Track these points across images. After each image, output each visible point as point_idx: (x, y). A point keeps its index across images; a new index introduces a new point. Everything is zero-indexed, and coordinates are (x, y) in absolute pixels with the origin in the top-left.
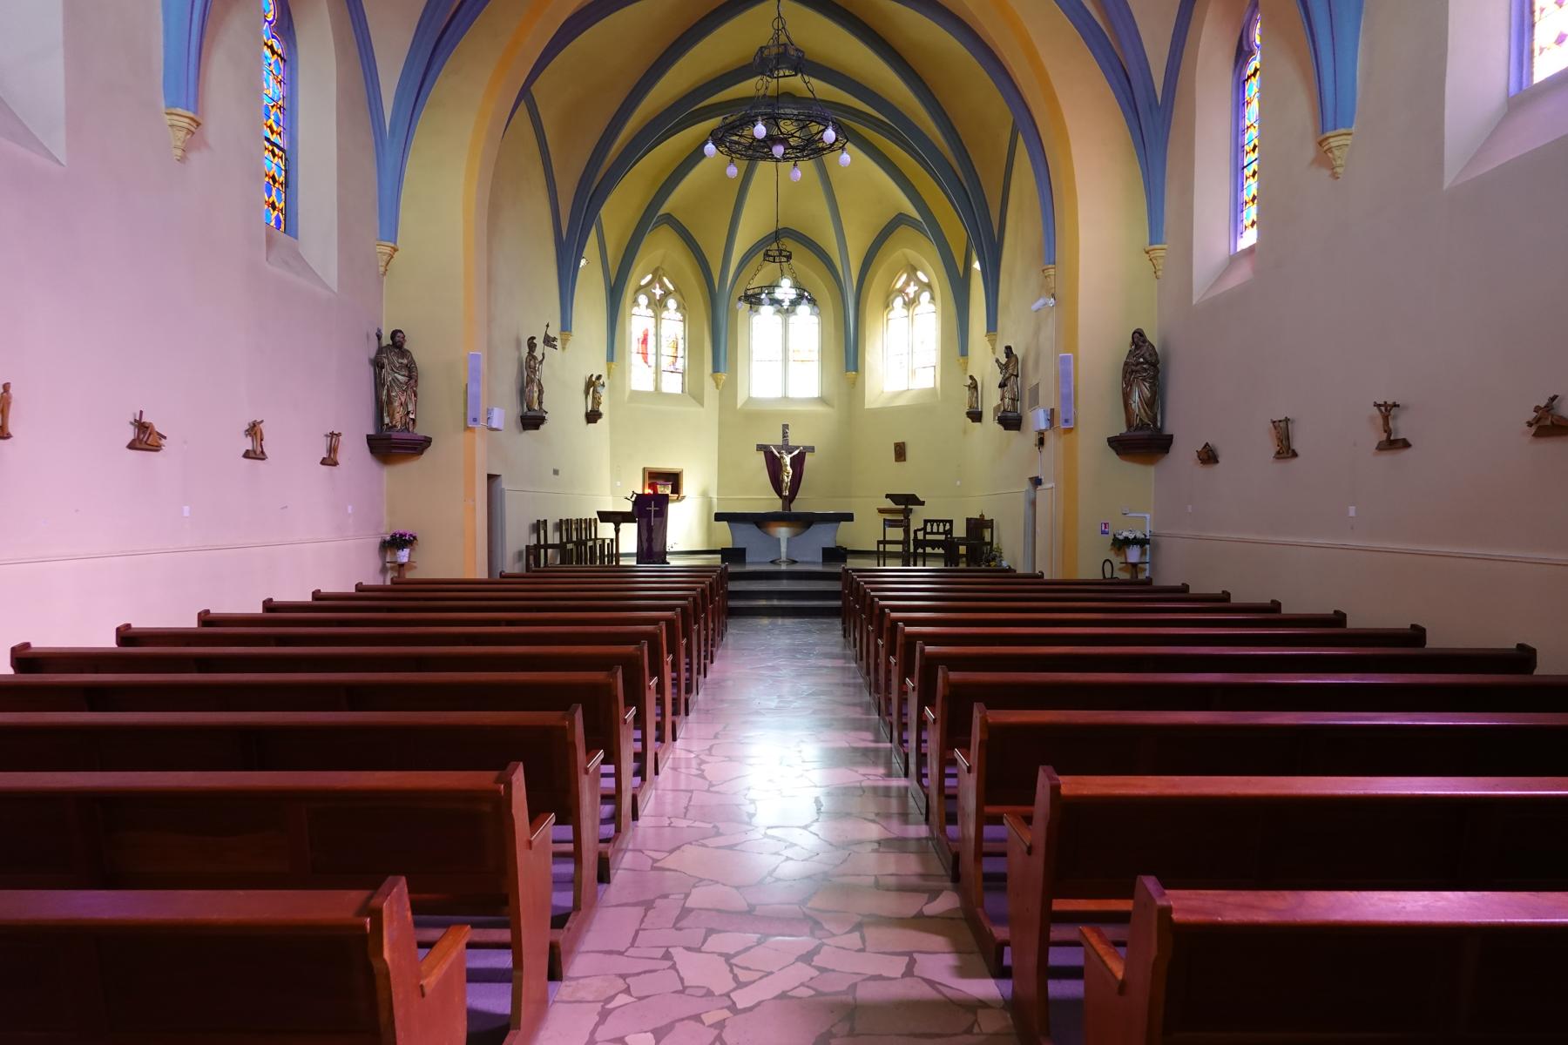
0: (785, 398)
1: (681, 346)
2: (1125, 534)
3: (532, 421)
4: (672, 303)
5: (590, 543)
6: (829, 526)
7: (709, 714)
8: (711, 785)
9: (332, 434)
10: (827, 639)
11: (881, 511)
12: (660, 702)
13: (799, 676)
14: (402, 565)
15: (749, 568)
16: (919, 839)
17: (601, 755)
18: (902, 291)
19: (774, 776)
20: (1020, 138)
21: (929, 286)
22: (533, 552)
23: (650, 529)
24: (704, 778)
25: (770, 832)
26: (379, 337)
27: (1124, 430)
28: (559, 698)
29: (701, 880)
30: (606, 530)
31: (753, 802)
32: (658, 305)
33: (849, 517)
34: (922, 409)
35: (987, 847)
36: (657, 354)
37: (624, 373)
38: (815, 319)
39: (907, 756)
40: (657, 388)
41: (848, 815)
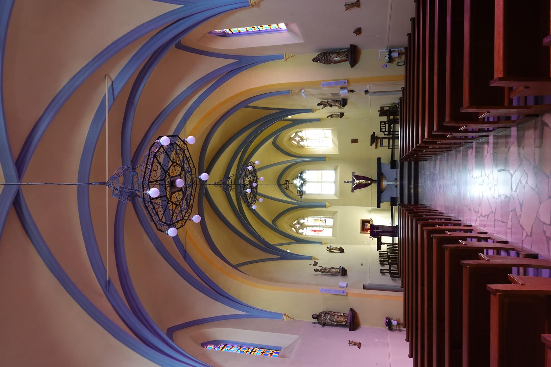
0: (335, 182)
1: (317, 218)
2: (387, 58)
3: (343, 272)
4: (302, 221)
5: (389, 254)
6: (382, 166)
7: (460, 211)
8: (492, 212)
9: (349, 343)
10: (427, 167)
11: (376, 147)
12: (455, 230)
13: (443, 177)
14: (398, 324)
15: (399, 195)
16: (518, 131)
17: (481, 254)
18: (298, 142)
19: (483, 187)
20: (250, 105)
21: (296, 133)
22: (392, 275)
23: (384, 232)
24: (489, 215)
25: (514, 189)
26: (315, 323)
27: (348, 62)
28: (457, 270)
29: (537, 217)
30: (384, 248)
31: (500, 196)
32: (303, 226)
33: (379, 159)
34: (339, 134)
35: (522, 103)
36: (319, 227)
37: (326, 238)
38: (307, 172)
39: (479, 136)
40: (331, 227)
41: (506, 159)
